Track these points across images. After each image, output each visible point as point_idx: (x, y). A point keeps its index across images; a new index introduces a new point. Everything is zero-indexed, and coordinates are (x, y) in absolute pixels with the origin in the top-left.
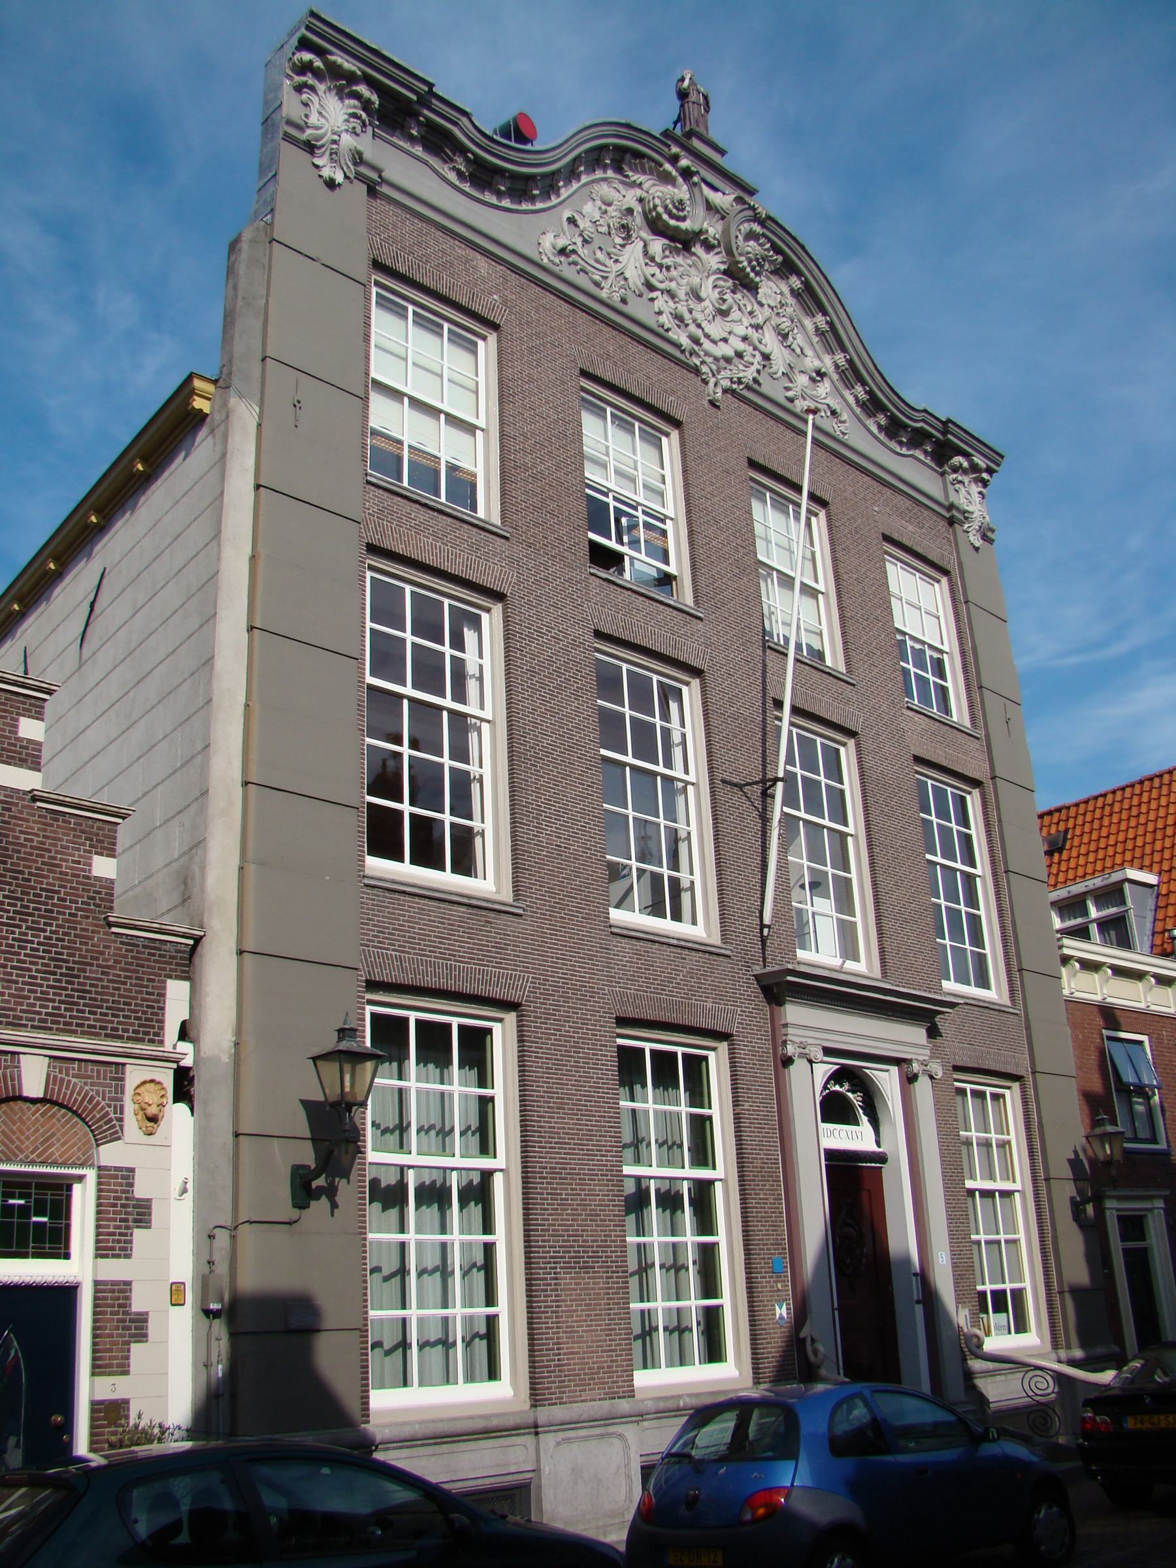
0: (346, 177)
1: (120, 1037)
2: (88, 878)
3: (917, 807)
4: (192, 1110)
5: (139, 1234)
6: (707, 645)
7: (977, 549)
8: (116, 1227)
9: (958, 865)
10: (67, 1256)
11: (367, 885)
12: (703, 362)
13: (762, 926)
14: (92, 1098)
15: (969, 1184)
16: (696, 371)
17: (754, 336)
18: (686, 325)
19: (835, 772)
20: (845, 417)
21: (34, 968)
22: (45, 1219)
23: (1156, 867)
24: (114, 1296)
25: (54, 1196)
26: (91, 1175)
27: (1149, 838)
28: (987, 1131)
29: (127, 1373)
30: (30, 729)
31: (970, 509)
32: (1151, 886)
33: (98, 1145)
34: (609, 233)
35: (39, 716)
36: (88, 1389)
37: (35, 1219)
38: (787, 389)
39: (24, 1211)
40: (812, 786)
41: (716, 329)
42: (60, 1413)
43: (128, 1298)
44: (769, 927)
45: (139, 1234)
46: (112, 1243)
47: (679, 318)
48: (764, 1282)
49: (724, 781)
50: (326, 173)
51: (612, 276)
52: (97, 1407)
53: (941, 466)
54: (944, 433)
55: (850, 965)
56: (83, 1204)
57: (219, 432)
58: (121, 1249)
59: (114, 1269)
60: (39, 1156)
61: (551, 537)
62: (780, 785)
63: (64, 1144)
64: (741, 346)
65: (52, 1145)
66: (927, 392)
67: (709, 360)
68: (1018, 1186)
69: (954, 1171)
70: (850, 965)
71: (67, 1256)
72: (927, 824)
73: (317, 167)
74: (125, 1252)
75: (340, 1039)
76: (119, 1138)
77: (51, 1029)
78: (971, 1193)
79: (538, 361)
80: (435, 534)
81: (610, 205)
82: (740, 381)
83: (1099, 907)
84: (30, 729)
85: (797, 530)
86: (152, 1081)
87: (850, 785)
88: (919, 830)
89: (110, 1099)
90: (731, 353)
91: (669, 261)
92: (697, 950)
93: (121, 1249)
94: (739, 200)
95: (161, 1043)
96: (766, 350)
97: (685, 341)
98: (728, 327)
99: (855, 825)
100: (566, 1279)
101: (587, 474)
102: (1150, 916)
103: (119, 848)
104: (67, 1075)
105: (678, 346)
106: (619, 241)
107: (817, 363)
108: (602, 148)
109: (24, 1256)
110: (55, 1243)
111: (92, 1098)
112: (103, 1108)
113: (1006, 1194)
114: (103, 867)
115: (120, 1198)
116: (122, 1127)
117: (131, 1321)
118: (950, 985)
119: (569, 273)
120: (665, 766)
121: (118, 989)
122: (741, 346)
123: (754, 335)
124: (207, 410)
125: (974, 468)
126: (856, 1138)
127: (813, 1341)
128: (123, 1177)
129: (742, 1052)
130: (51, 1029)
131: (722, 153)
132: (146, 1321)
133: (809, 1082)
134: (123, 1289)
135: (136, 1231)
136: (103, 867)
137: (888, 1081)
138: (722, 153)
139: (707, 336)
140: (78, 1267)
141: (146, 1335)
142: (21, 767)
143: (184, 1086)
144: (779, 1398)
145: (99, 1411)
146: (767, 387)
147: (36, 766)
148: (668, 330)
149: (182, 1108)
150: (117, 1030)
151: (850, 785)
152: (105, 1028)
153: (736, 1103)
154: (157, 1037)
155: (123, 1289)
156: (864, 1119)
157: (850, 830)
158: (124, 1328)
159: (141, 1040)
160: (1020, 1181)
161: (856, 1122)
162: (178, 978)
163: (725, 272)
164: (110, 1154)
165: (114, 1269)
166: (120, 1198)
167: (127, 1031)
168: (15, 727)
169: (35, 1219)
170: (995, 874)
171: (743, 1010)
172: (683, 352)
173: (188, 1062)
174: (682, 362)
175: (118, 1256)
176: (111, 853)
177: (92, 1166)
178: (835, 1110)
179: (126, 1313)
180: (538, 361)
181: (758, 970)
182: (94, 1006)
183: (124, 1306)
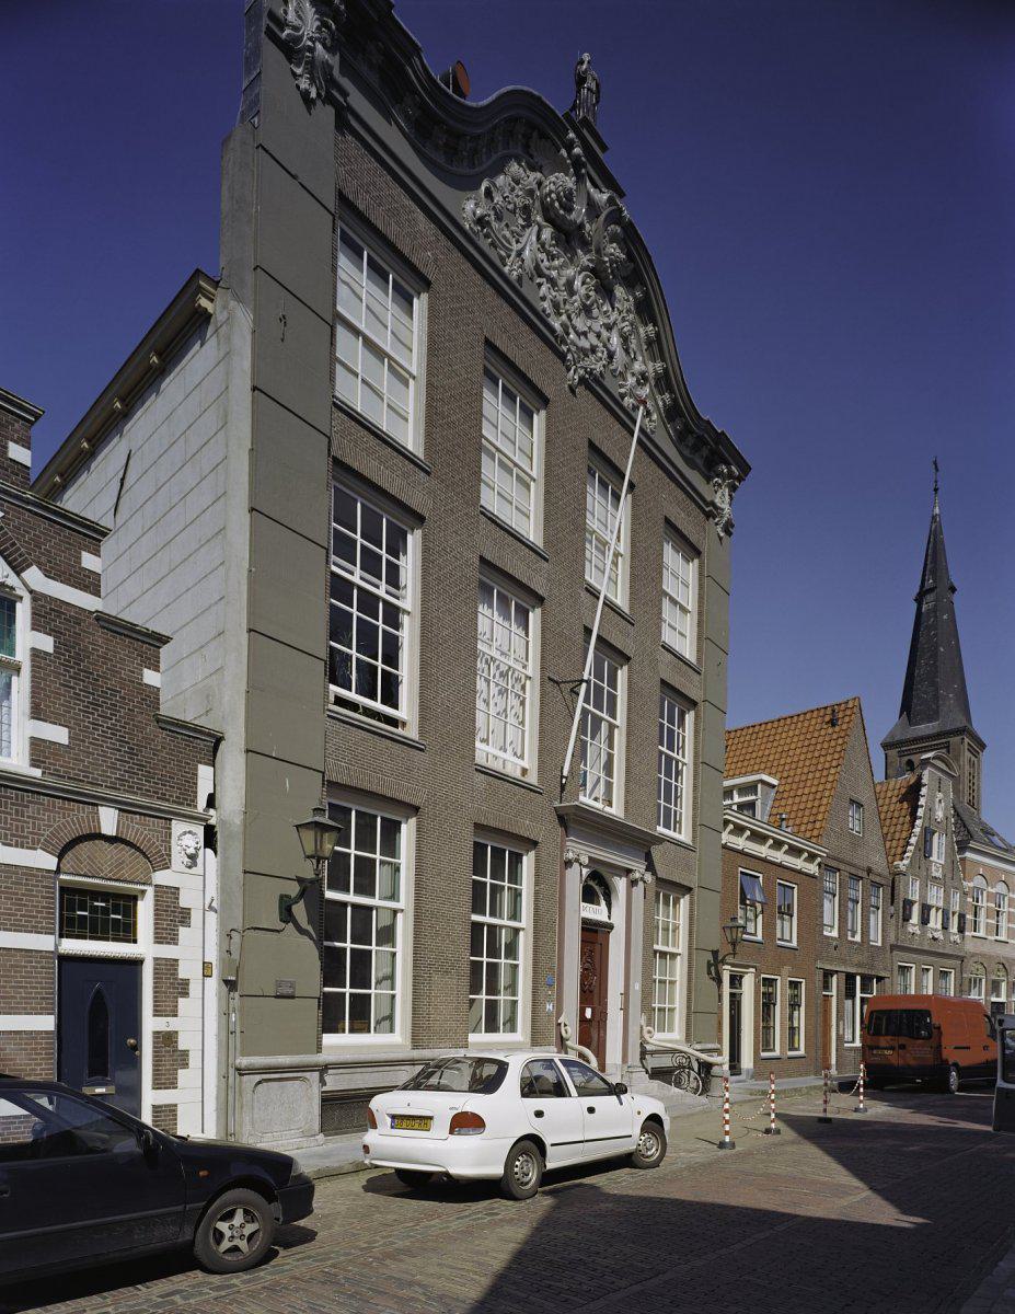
0: (319, 95)
1: (168, 800)
2: (140, 684)
3: (658, 714)
4: (216, 853)
5: (182, 931)
6: (549, 581)
7: (721, 539)
8: (168, 925)
9: (605, 716)
10: (135, 941)
11: (329, 716)
12: (569, 350)
13: (562, 777)
14: (150, 839)
15: (656, 947)
16: (562, 357)
17: (606, 333)
18: (561, 315)
19: (613, 683)
20: (655, 417)
21: (105, 745)
22: (120, 917)
23: (779, 775)
24: (166, 968)
25: (128, 902)
26: (150, 891)
27: (777, 756)
28: (668, 918)
29: (176, 1016)
30: (89, 561)
31: (723, 506)
32: (774, 786)
33: (155, 871)
34: (515, 213)
35: (97, 553)
36: (150, 1024)
37: (112, 916)
38: (621, 386)
39: (105, 911)
40: (599, 690)
41: (580, 323)
42: (133, 1038)
43: (176, 970)
44: (566, 778)
45: (182, 931)
46: (165, 935)
47: (556, 305)
48: (543, 990)
49: (550, 679)
50: (304, 84)
51: (513, 254)
52: (156, 1034)
53: (709, 470)
54: (716, 444)
55: (607, 809)
56: (145, 911)
57: (223, 330)
58: (172, 939)
59: (167, 951)
60: (114, 875)
61: (457, 477)
62: (584, 685)
63: (132, 868)
64: (595, 341)
65: (123, 868)
66: (713, 411)
67: (573, 349)
68: (680, 951)
69: (649, 938)
70: (607, 809)
71: (135, 941)
72: (662, 725)
73: (294, 74)
74: (174, 940)
75: (314, 815)
76: (168, 868)
77: (119, 789)
78: (656, 952)
79: (457, 322)
80: (379, 458)
81: (517, 183)
82: (591, 373)
83: (740, 795)
84: (89, 561)
85: (518, 642)
86: (190, 832)
87: (621, 693)
88: (657, 728)
89: (162, 841)
90: (587, 345)
91: (554, 251)
92: (523, 787)
93: (172, 939)
94: (611, 201)
95: (196, 807)
96: (613, 349)
97: (557, 326)
98: (589, 323)
99: (621, 719)
100: (436, 978)
101: (484, 432)
102: (770, 803)
103: (162, 666)
104: (132, 822)
105: (552, 331)
106: (521, 221)
107: (643, 367)
108: (514, 120)
109: (107, 939)
110: (127, 932)
111: (150, 839)
112: (157, 847)
113: (673, 956)
114: (150, 677)
115: (170, 907)
116: (170, 860)
117: (178, 984)
118: (661, 829)
119: (484, 244)
120: (668, 748)
121: (165, 767)
122: (595, 341)
123: (605, 334)
124: (210, 310)
125: (730, 475)
126: (597, 912)
127: (565, 1025)
128: (172, 893)
129: (543, 854)
130: (119, 789)
131: (604, 148)
132: (188, 984)
133: (575, 879)
134: (173, 964)
135: (181, 928)
136: (150, 677)
137: (620, 884)
138: (604, 148)
139: (574, 328)
140: (144, 947)
141: (188, 994)
142: (85, 591)
143: (210, 839)
144: (470, 232)
145: (159, 1038)
146: (608, 382)
147: (97, 593)
148: (548, 315)
149: (209, 851)
150: (165, 795)
151: (621, 693)
152: (157, 793)
153: (537, 884)
154: (193, 803)
155: (173, 964)
156: (603, 903)
157: (617, 723)
158: (174, 988)
159: (182, 804)
160: (681, 947)
161: (599, 904)
162: (206, 764)
163: (593, 271)
164: (161, 878)
165: (167, 951)
166: (170, 907)
167: (172, 796)
168: (78, 559)
169: (112, 916)
170: (695, 764)
171: (542, 827)
172: (556, 338)
173: (212, 822)
174: (553, 344)
175: (169, 943)
176: (157, 669)
177: (150, 884)
178: (589, 896)
179: (176, 979)
180: (457, 322)
181: (557, 804)
182: (149, 776)
183: (174, 974)
